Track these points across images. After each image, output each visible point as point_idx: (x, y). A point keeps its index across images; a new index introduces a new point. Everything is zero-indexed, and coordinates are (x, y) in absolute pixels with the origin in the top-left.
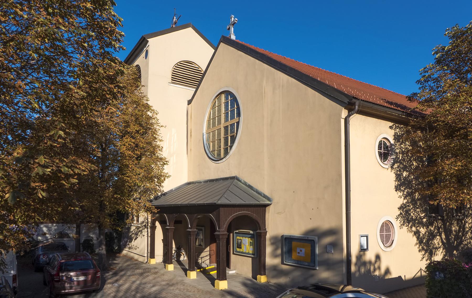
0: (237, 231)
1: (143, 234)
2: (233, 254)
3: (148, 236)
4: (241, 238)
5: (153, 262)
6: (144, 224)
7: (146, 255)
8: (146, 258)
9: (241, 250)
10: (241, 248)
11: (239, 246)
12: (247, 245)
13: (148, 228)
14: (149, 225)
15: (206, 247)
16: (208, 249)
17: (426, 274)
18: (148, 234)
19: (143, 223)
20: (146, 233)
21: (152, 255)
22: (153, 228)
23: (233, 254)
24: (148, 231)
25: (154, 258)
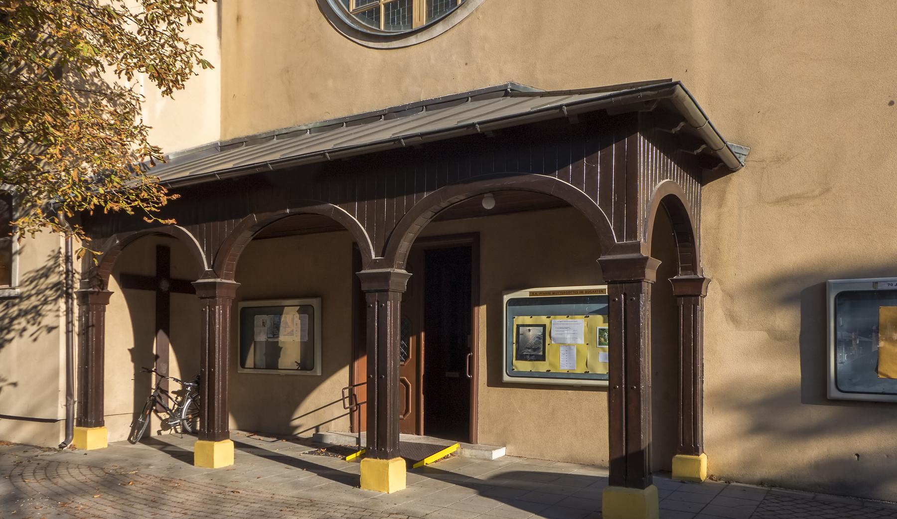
0: (524, 294)
1: (48, 320)
2: (495, 380)
3: (68, 332)
4: (544, 320)
5: (96, 440)
6: (53, 279)
7: (61, 414)
8: (62, 425)
9: (542, 367)
10: (543, 358)
11: (535, 351)
12: (577, 339)
13: (69, 296)
14: (77, 285)
15: (327, 374)
16: (343, 376)
17: (642, 447)
18: (69, 323)
19: (46, 276)
20: (62, 321)
21: (90, 410)
22: (93, 301)
23: (495, 380)
24: (69, 311)
25: (100, 423)
